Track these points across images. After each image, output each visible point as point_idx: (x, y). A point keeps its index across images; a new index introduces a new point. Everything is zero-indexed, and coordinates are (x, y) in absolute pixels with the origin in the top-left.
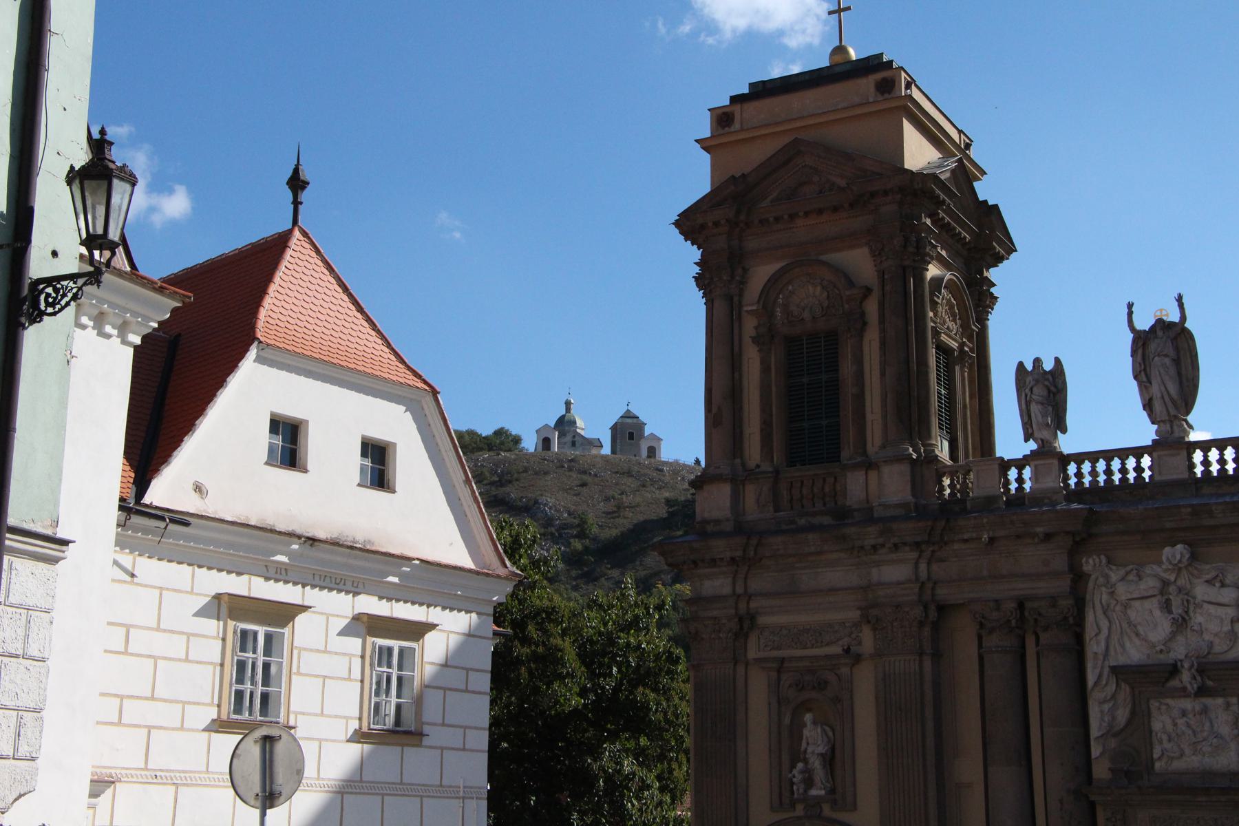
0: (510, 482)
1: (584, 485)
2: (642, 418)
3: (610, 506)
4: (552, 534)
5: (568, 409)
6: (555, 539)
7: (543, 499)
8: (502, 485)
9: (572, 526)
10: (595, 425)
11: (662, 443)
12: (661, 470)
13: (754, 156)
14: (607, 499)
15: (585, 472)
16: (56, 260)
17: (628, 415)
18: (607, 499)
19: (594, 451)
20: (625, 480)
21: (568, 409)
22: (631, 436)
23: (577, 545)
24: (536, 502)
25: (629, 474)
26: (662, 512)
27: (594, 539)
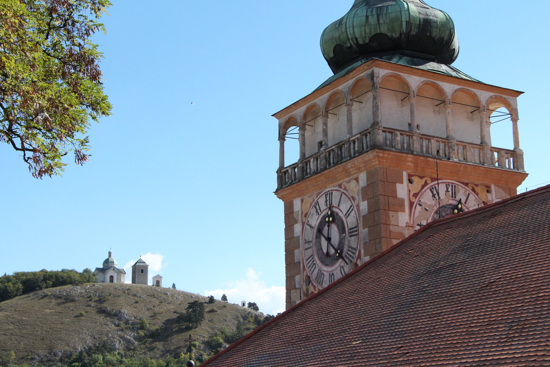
0: (105, 301)
1: (137, 302)
2: (147, 263)
3: (151, 313)
4: (130, 328)
5: (110, 256)
6: (132, 329)
7: (123, 311)
8: (101, 303)
9: (137, 324)
10: (125, 264)
11: (163, 279)
12: (167, 294)
13: (401, 56)
14: (148, 309)
15: (135, 295)
16: (86, 163)
17: (140, 261)
18: (148, 309)
19: (201, 333)
20: (153, 299)
21: (110, 256)
22: (142, 271)
23: (142, 333)
24: (120, 312)
25: (153, 296)
26: (175, 316)
27: (148, 330)
